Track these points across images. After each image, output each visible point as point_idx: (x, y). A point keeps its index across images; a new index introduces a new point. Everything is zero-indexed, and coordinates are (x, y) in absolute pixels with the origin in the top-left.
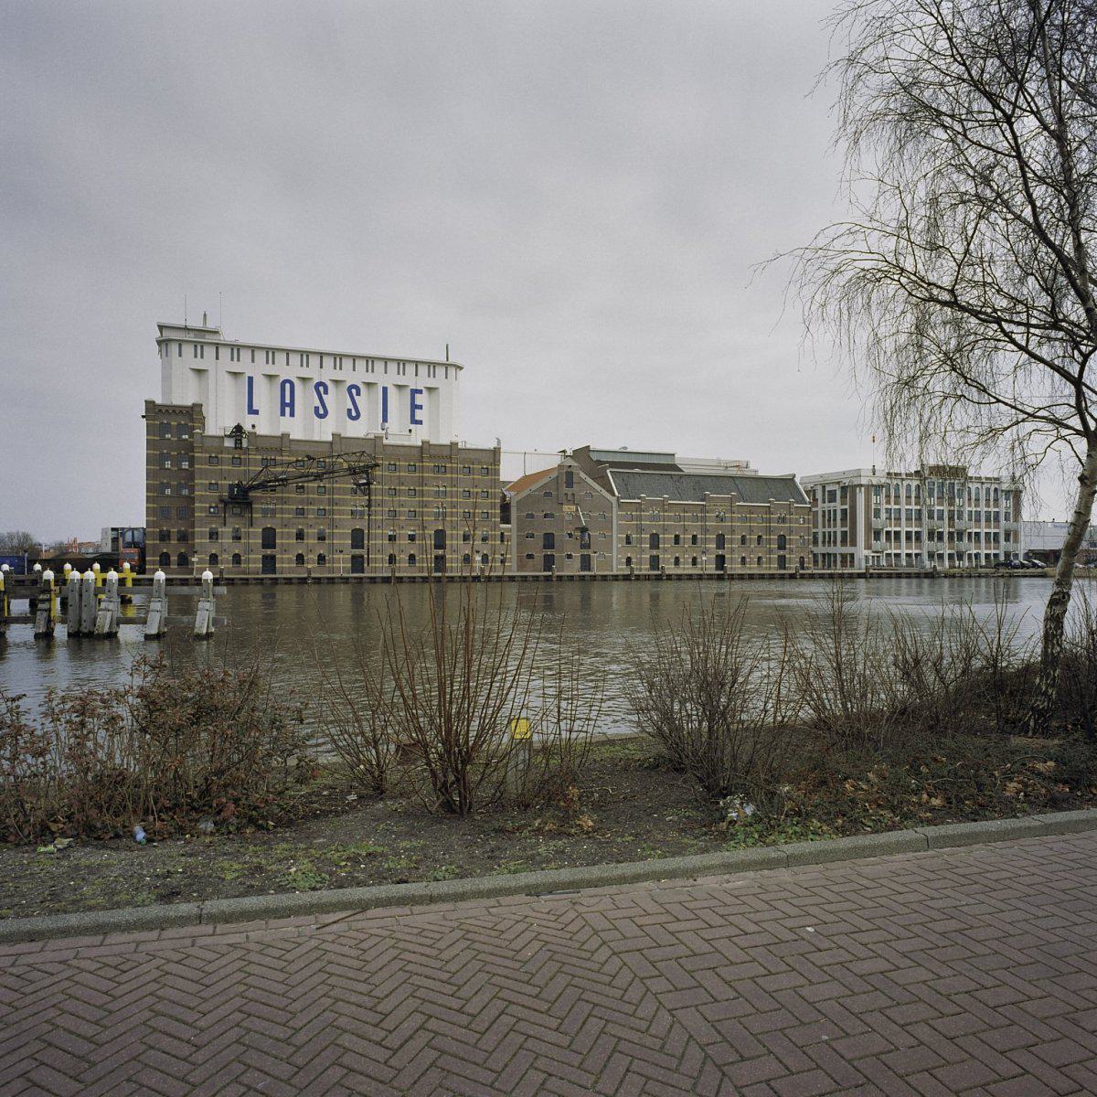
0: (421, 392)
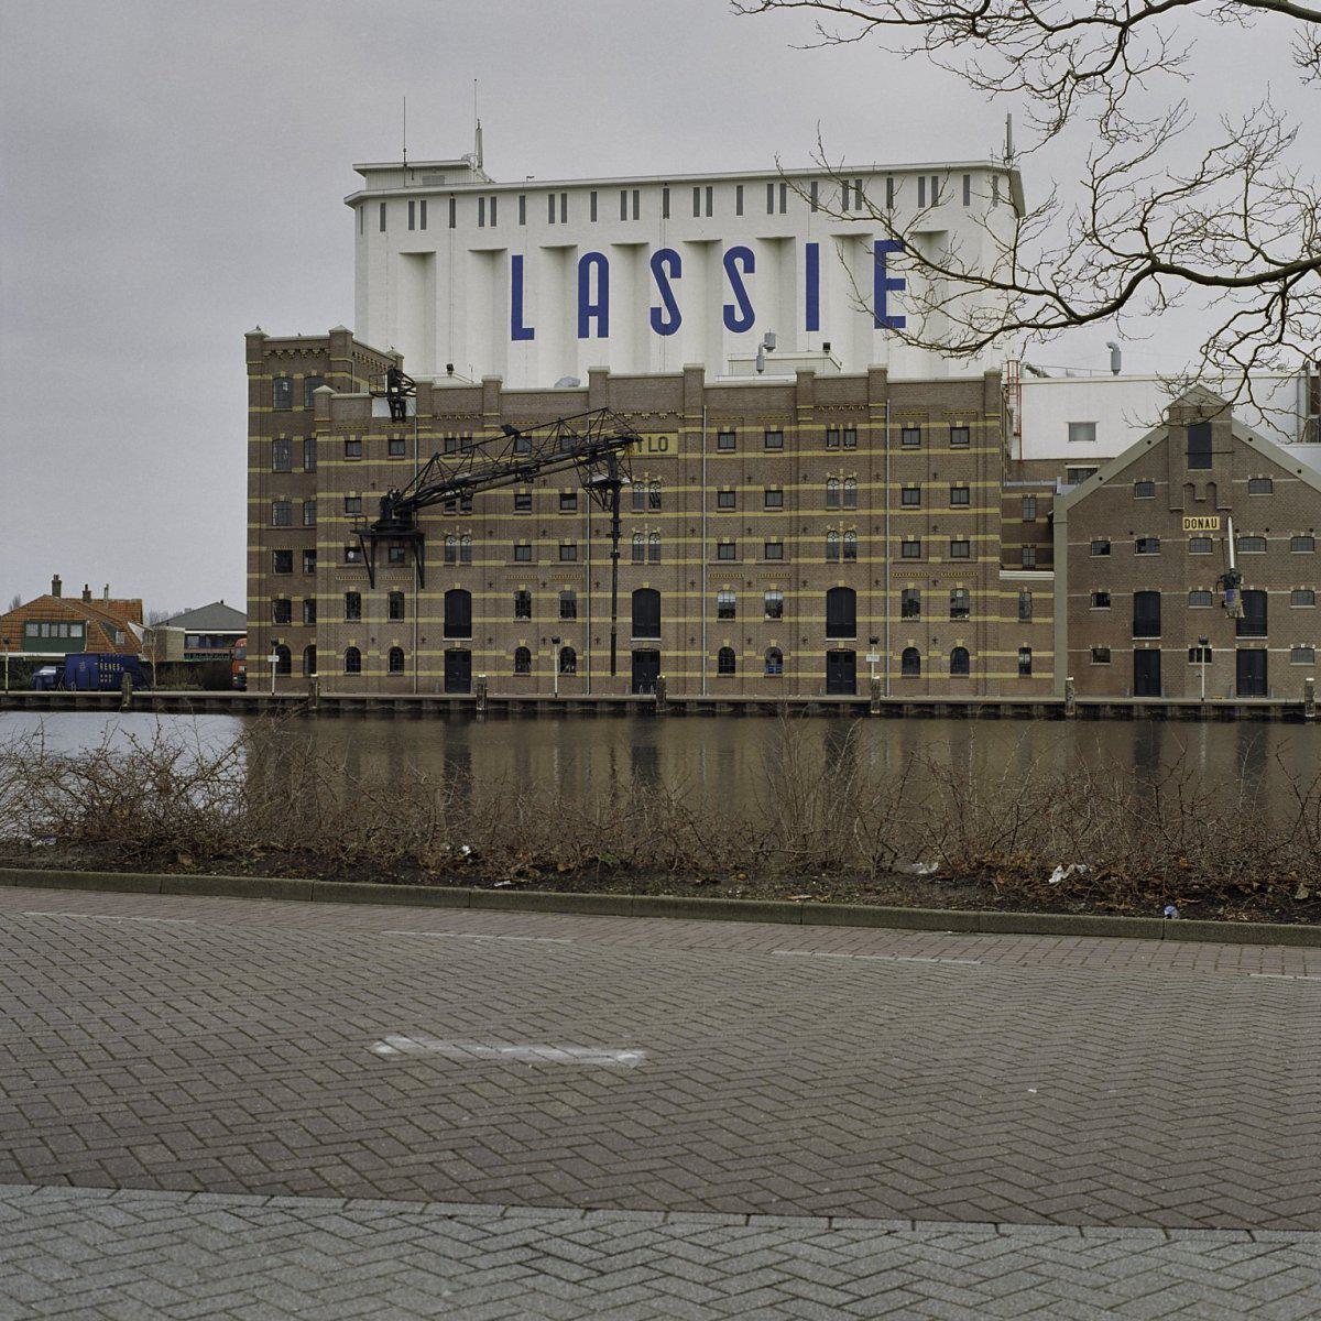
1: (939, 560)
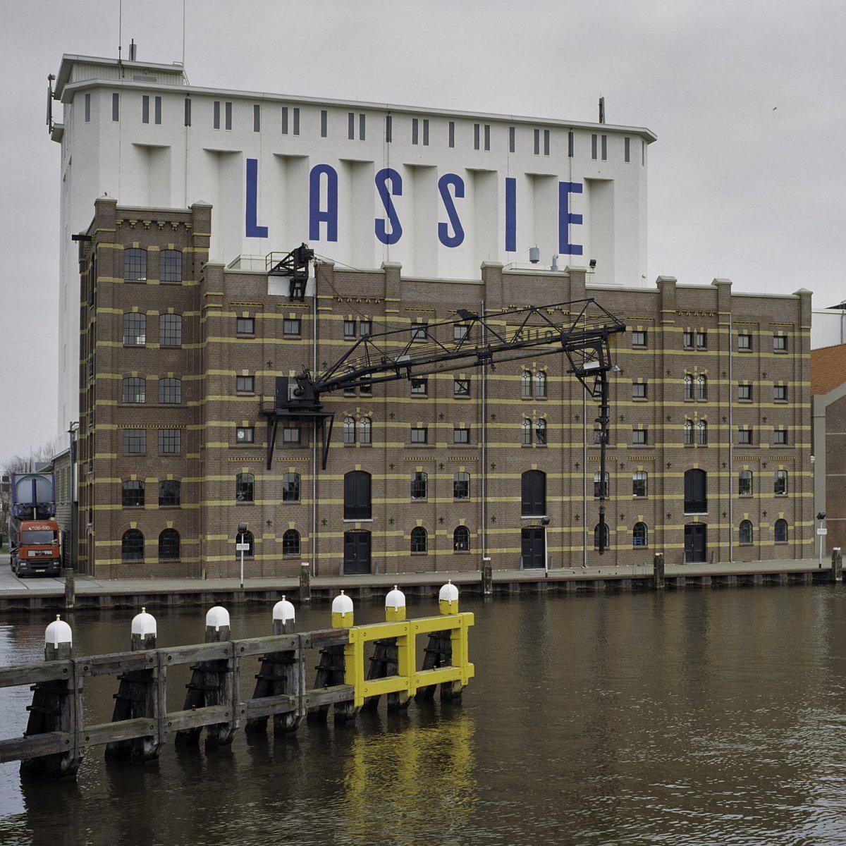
0: (577, 188)
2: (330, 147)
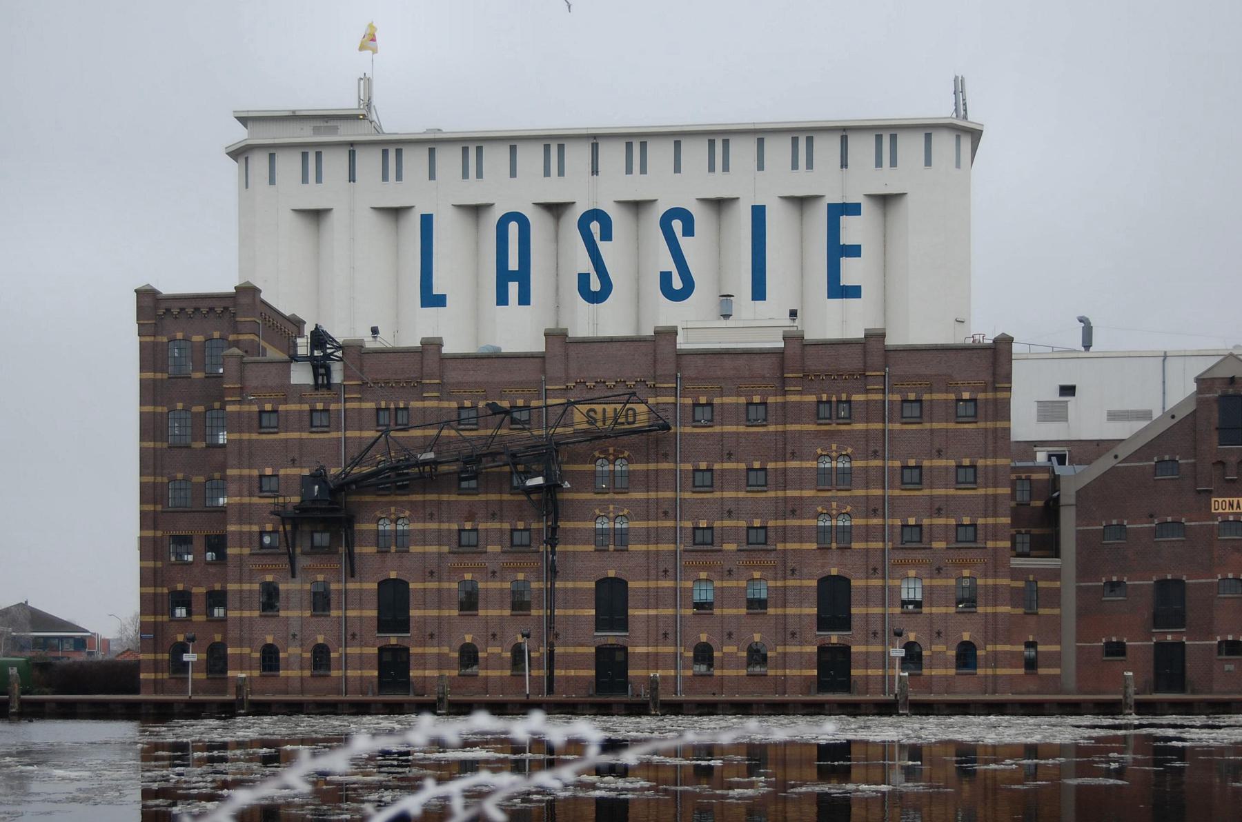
0: (854, 209)
1: (943, 545)
2: (516, 189)
